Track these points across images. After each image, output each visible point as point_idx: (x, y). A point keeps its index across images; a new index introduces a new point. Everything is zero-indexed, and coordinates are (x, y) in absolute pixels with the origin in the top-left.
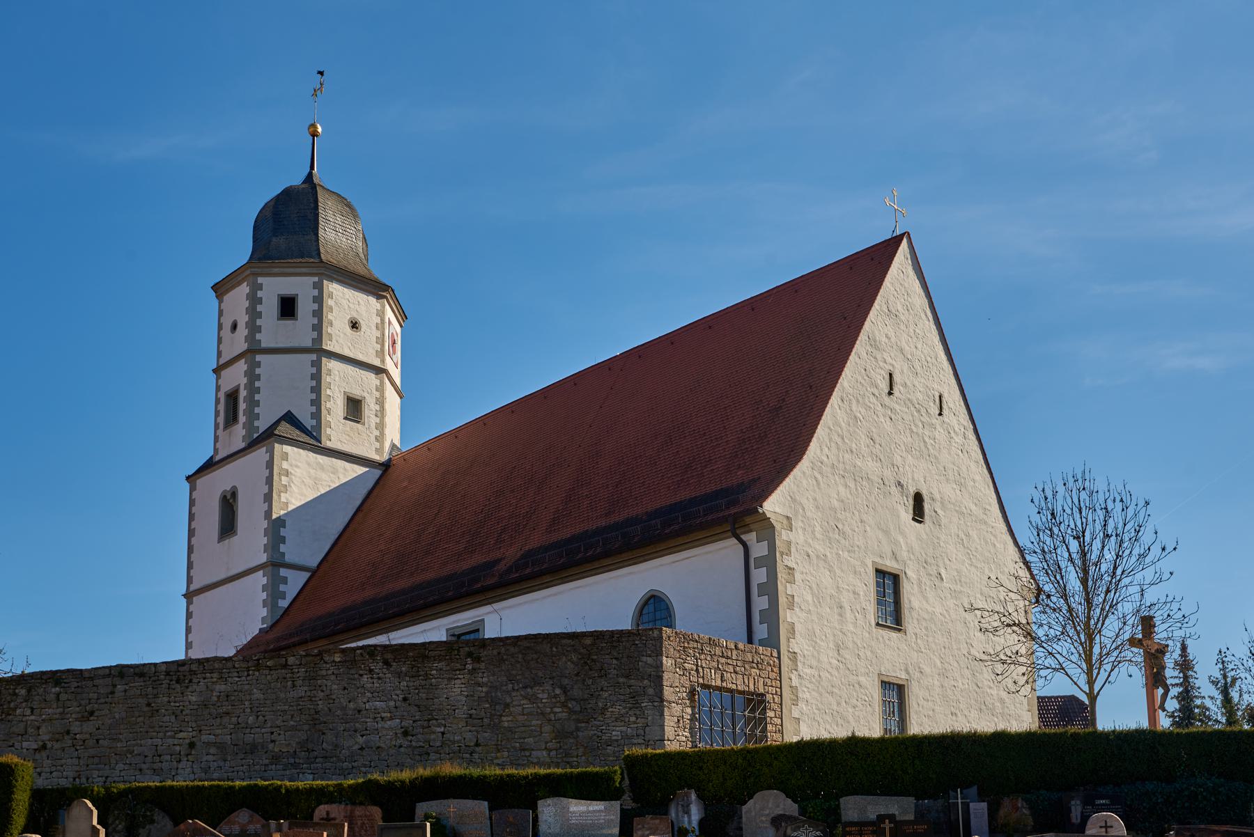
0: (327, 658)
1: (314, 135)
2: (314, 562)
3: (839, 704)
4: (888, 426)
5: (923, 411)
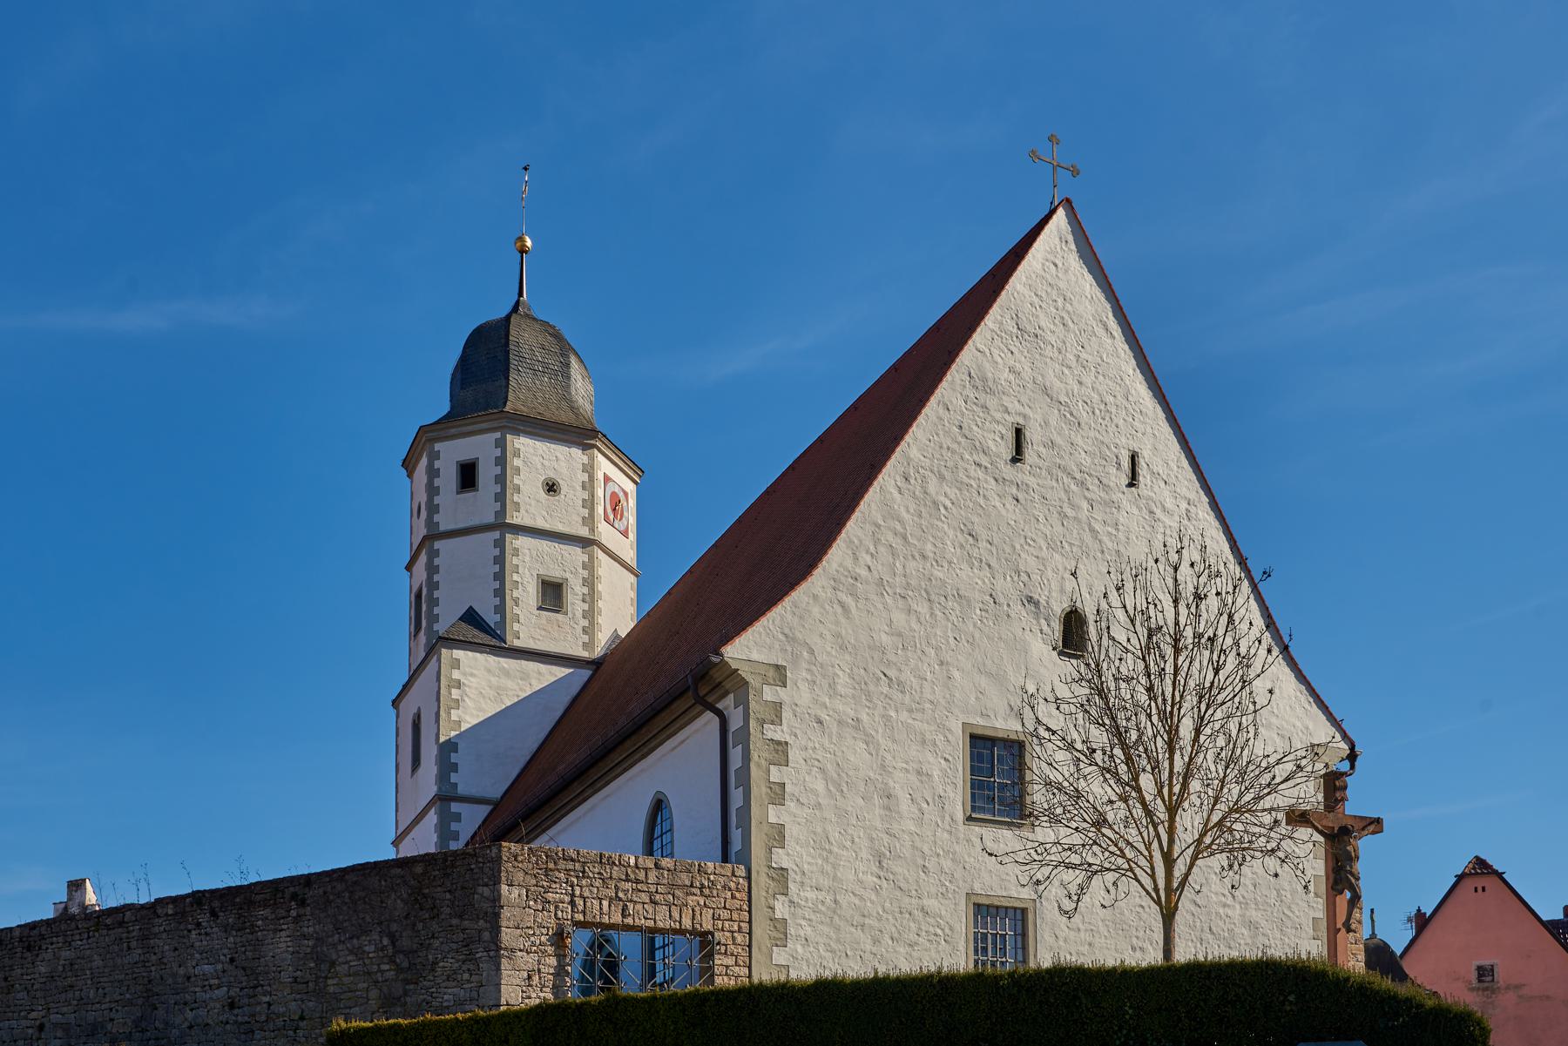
0: (159, 911)
1: (523, 251)
2: (496, 792)
3: (876, 941)
4: (1010, 512)
5: (1092, 483)
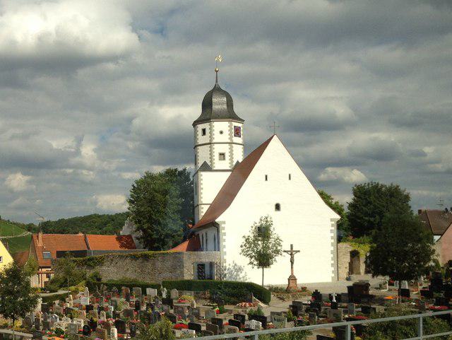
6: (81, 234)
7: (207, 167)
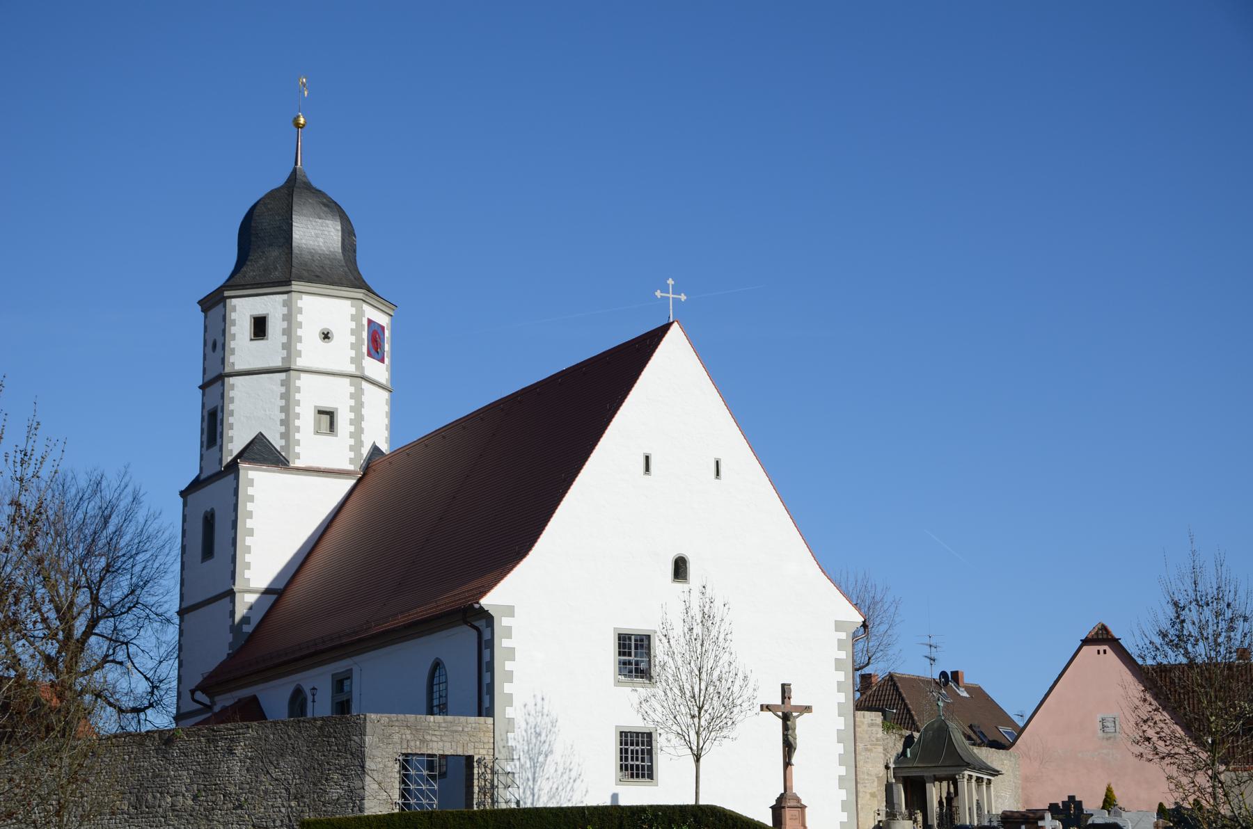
1: (297, 125)
6: (1225, 810)
7: (262, 452)
